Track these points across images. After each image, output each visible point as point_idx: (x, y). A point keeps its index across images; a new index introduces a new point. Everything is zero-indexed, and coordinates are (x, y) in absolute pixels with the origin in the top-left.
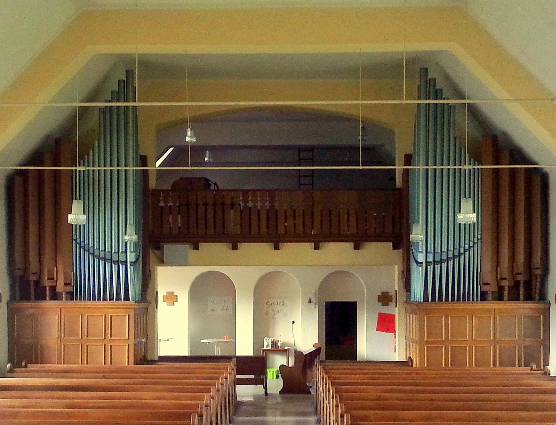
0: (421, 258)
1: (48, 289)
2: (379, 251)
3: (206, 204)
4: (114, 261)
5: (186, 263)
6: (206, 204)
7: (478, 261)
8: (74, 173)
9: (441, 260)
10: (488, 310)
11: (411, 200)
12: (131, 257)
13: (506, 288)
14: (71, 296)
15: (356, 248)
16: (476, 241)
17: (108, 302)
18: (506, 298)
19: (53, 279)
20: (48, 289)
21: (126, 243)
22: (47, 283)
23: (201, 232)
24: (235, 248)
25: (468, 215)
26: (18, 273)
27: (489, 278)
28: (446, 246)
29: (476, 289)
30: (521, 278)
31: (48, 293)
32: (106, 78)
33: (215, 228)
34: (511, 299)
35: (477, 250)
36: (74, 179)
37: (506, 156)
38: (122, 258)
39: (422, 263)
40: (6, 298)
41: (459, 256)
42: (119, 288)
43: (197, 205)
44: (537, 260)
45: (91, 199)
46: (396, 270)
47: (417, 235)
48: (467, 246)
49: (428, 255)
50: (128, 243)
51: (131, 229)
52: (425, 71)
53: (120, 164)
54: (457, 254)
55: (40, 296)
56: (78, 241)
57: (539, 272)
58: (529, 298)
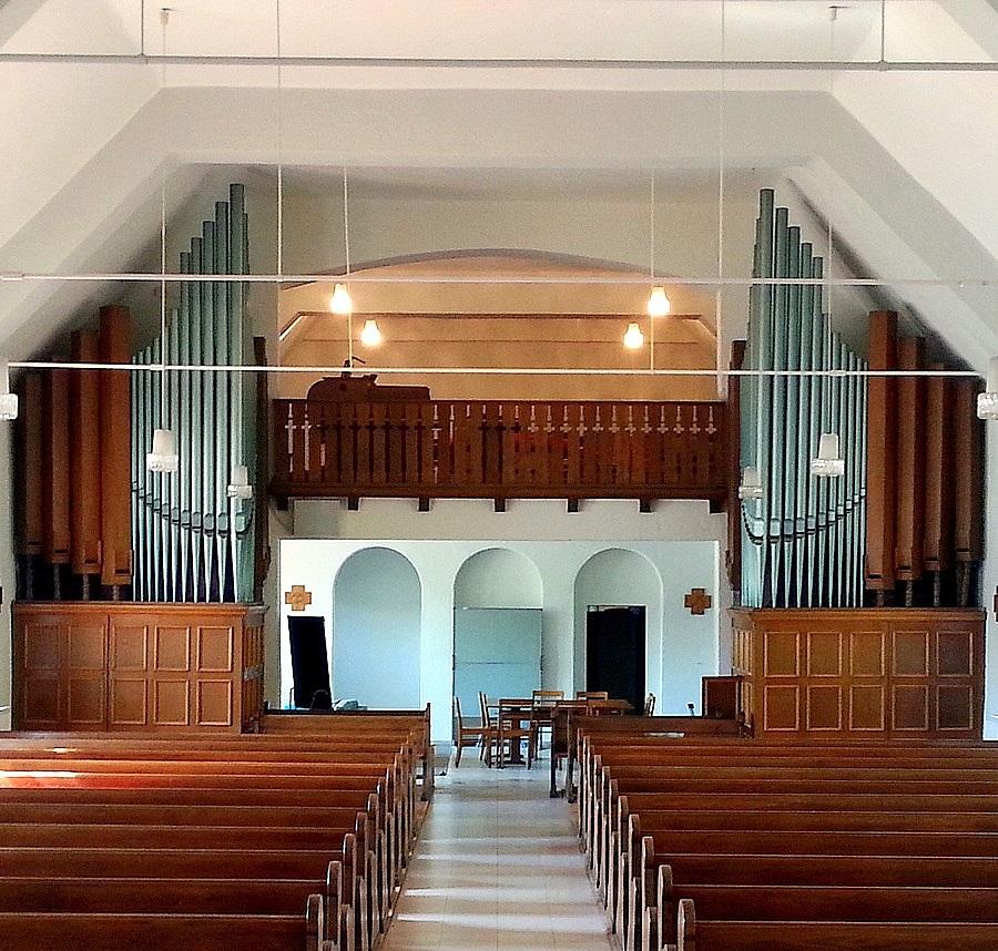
0: (759, 529)
1: (56, 571)
2: (687, 513)
3: (371, 427)
4: (207, 531)
5: (334, 534)
6: (371, 427)
7: (860, 535)
8: (134, 378)
9: (795, 533)
10: (876, 625)
11: (743, 418)
12: (237, 524)
13: (910, 585)
14: (126, 593)
15: (645, 508)
16: (857, 500)
17: (195, 606)
18: (908, 602)
19: (128, 571)
20: (56, 571)
21: (229, 499)
22: (87, 570)
23: (363, 476)
24: (424, 507)
25: (829, 462)
26: (31, 550)
27: (877, 567)
28: (805, 508)
29: (855, 587)
30: (935, 566)
31: (86, 586)
32: (193, 198)
33: (387, 470)
34: (917, 603)
35: (860, 514)
36: (134, 382)
37: (911, 353)
38: (221, 525)
39: (761, 538)
40: (9, 595)
41: (827, 526)
42: (215, 581)
43: (355, 427)
44: (964, 533)
45: (149, 395)
46: (716, 550)
47: (752, 485)
48: (841, 509)
49: (772, 524)
50: (232, 500)
51: (240, 475)
52: (768, 195)
53: (219, 361)
54: (822, 523)
55: (72, 592)
56: (141, 493)
57: (967, 556)
58: (949, 600)
